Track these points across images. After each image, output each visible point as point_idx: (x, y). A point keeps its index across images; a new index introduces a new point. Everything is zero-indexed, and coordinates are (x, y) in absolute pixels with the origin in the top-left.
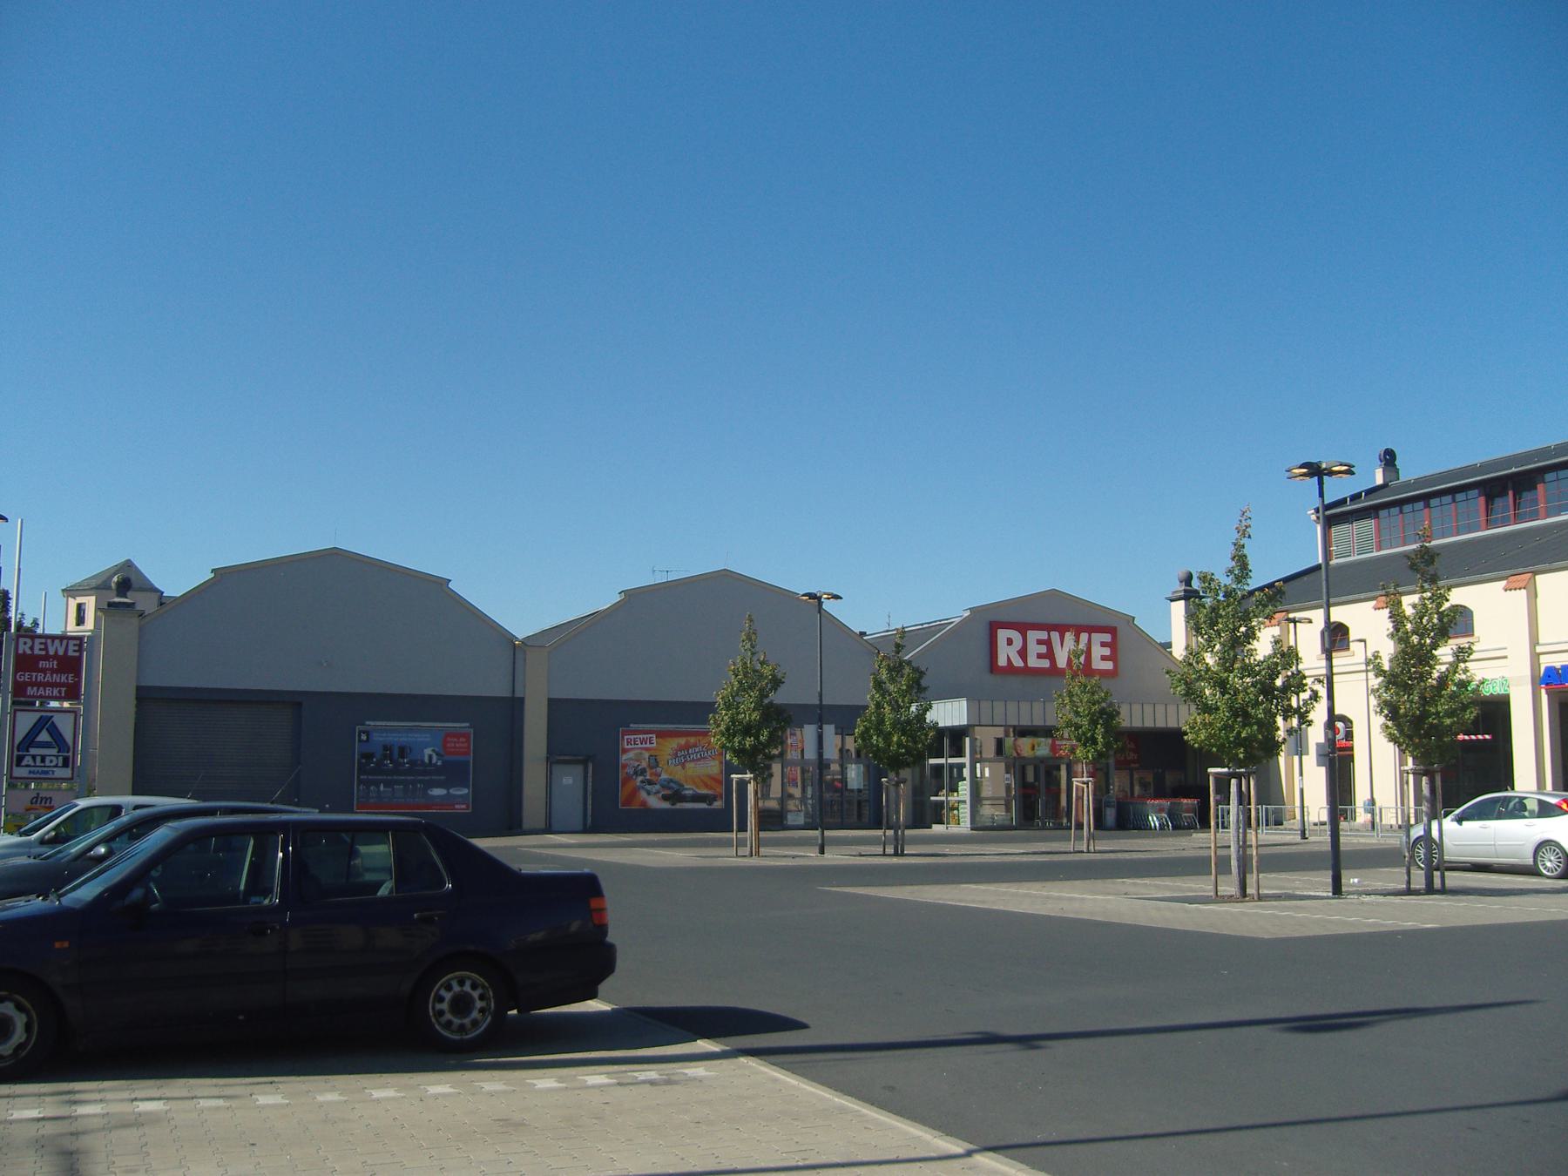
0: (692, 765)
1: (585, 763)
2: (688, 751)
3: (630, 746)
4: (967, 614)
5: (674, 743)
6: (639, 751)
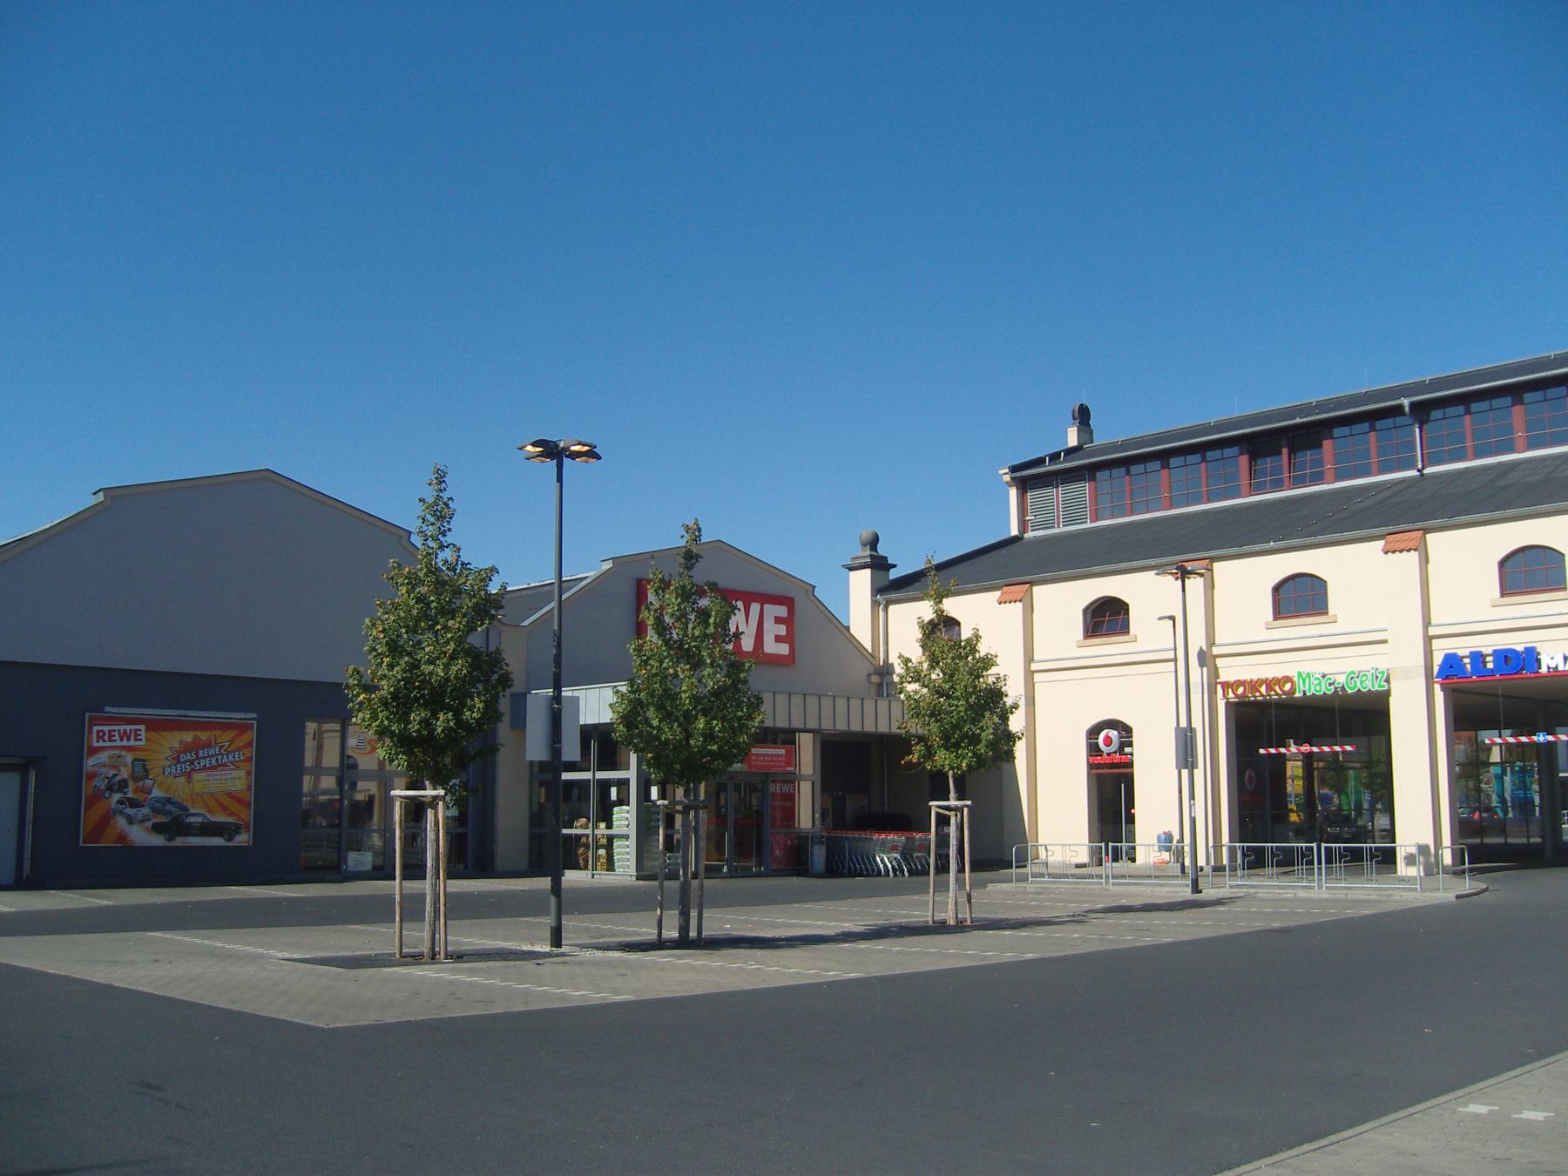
0: (203, 776)
1: (23, 769)
2: (197, 754)
3: (101, 744)
4: (608, 566)
5: (175, 739)
6: (117, 752)
